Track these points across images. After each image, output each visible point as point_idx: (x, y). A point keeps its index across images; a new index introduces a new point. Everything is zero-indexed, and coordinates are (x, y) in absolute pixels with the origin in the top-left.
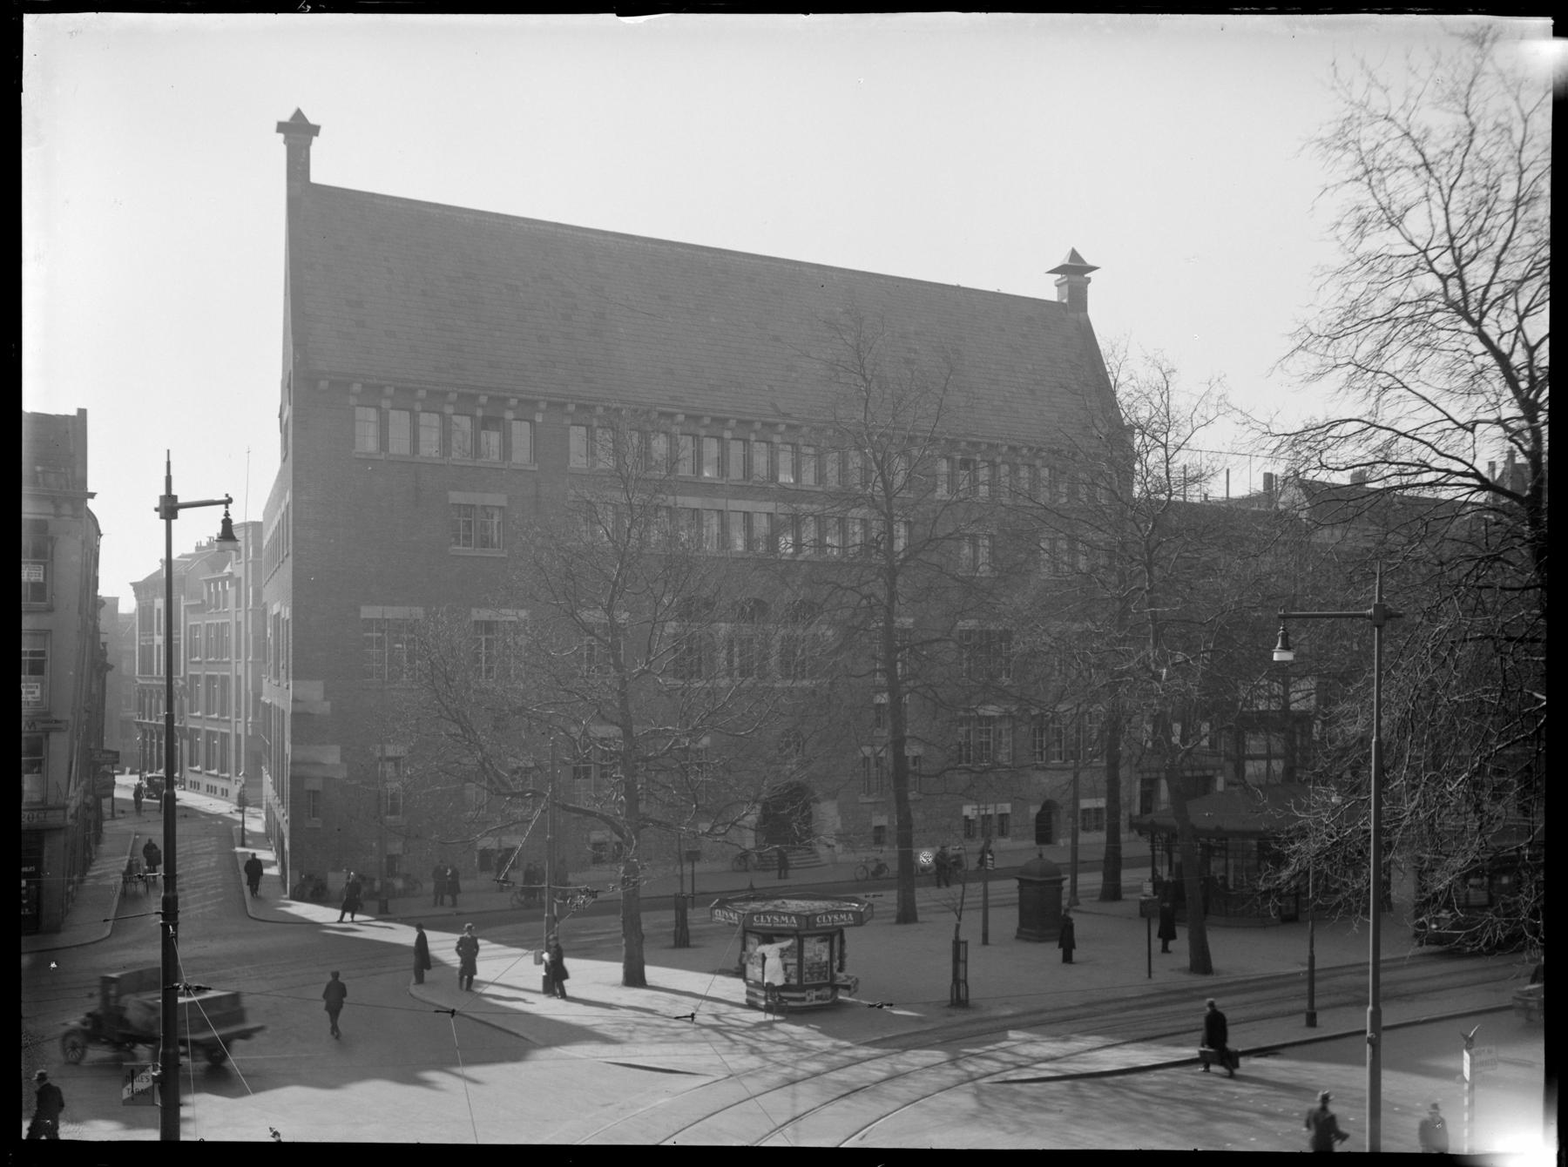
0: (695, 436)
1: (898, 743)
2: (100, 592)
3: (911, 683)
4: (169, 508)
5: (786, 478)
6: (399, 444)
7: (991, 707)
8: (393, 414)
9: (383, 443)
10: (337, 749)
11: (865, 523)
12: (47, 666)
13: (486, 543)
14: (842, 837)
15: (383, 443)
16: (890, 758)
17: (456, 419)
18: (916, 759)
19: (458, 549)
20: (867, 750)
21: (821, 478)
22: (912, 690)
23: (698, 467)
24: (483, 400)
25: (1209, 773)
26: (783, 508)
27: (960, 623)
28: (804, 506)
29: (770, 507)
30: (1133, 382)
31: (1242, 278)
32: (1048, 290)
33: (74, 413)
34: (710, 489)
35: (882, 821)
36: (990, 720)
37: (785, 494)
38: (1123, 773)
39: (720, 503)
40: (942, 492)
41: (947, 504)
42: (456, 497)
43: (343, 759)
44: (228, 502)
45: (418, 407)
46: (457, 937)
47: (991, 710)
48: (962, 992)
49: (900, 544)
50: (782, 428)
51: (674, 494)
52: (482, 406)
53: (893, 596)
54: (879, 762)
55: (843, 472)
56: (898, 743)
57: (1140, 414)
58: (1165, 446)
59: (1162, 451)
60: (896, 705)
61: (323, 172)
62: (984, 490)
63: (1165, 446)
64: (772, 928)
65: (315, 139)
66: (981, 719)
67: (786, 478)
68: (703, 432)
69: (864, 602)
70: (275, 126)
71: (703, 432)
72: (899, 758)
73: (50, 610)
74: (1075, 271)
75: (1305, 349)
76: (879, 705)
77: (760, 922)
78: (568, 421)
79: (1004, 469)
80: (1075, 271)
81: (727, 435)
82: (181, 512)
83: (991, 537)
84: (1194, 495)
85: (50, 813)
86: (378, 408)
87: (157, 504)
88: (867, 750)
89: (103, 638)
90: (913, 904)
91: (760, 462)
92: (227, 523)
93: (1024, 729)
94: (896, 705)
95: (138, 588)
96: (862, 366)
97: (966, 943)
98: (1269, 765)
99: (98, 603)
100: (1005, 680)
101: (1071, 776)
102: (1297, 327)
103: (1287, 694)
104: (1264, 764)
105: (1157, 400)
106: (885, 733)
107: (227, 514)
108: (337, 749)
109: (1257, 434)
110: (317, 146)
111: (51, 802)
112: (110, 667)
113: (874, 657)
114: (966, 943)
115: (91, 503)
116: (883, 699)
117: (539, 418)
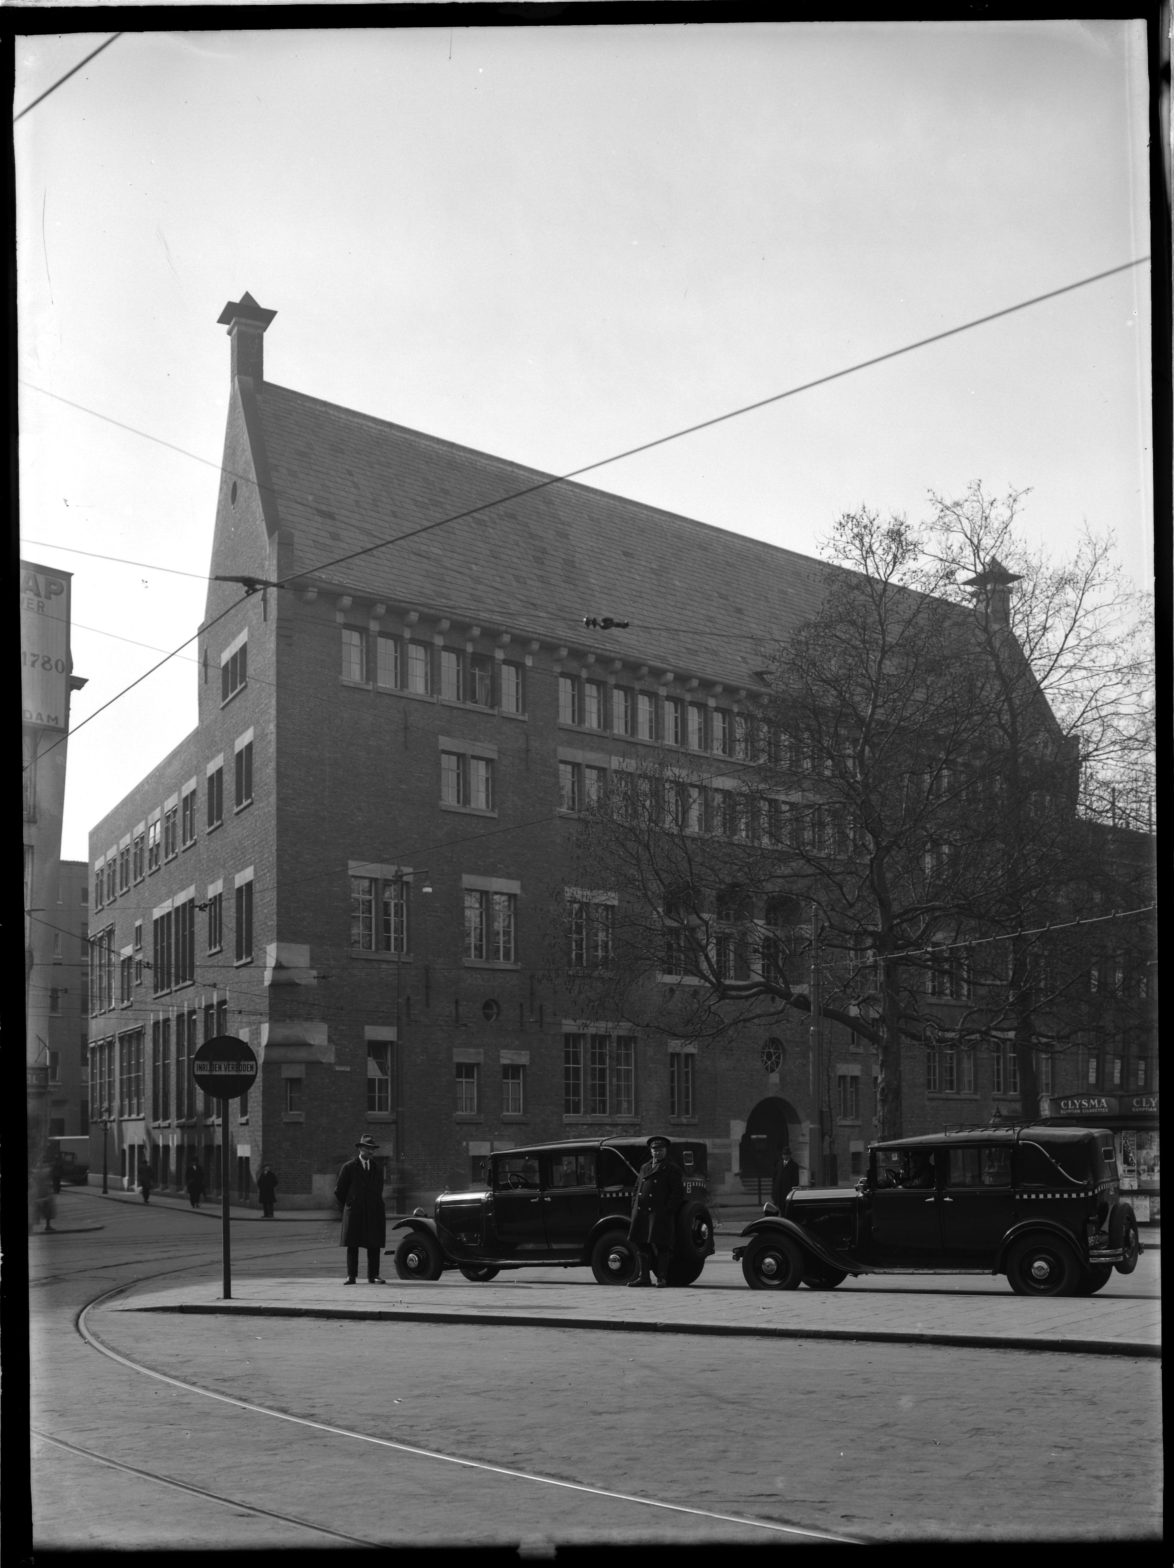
9: (370, 673)
34: (695, 761)
108: (324, 1027)
110: (271, 337)
117: (529, 662)
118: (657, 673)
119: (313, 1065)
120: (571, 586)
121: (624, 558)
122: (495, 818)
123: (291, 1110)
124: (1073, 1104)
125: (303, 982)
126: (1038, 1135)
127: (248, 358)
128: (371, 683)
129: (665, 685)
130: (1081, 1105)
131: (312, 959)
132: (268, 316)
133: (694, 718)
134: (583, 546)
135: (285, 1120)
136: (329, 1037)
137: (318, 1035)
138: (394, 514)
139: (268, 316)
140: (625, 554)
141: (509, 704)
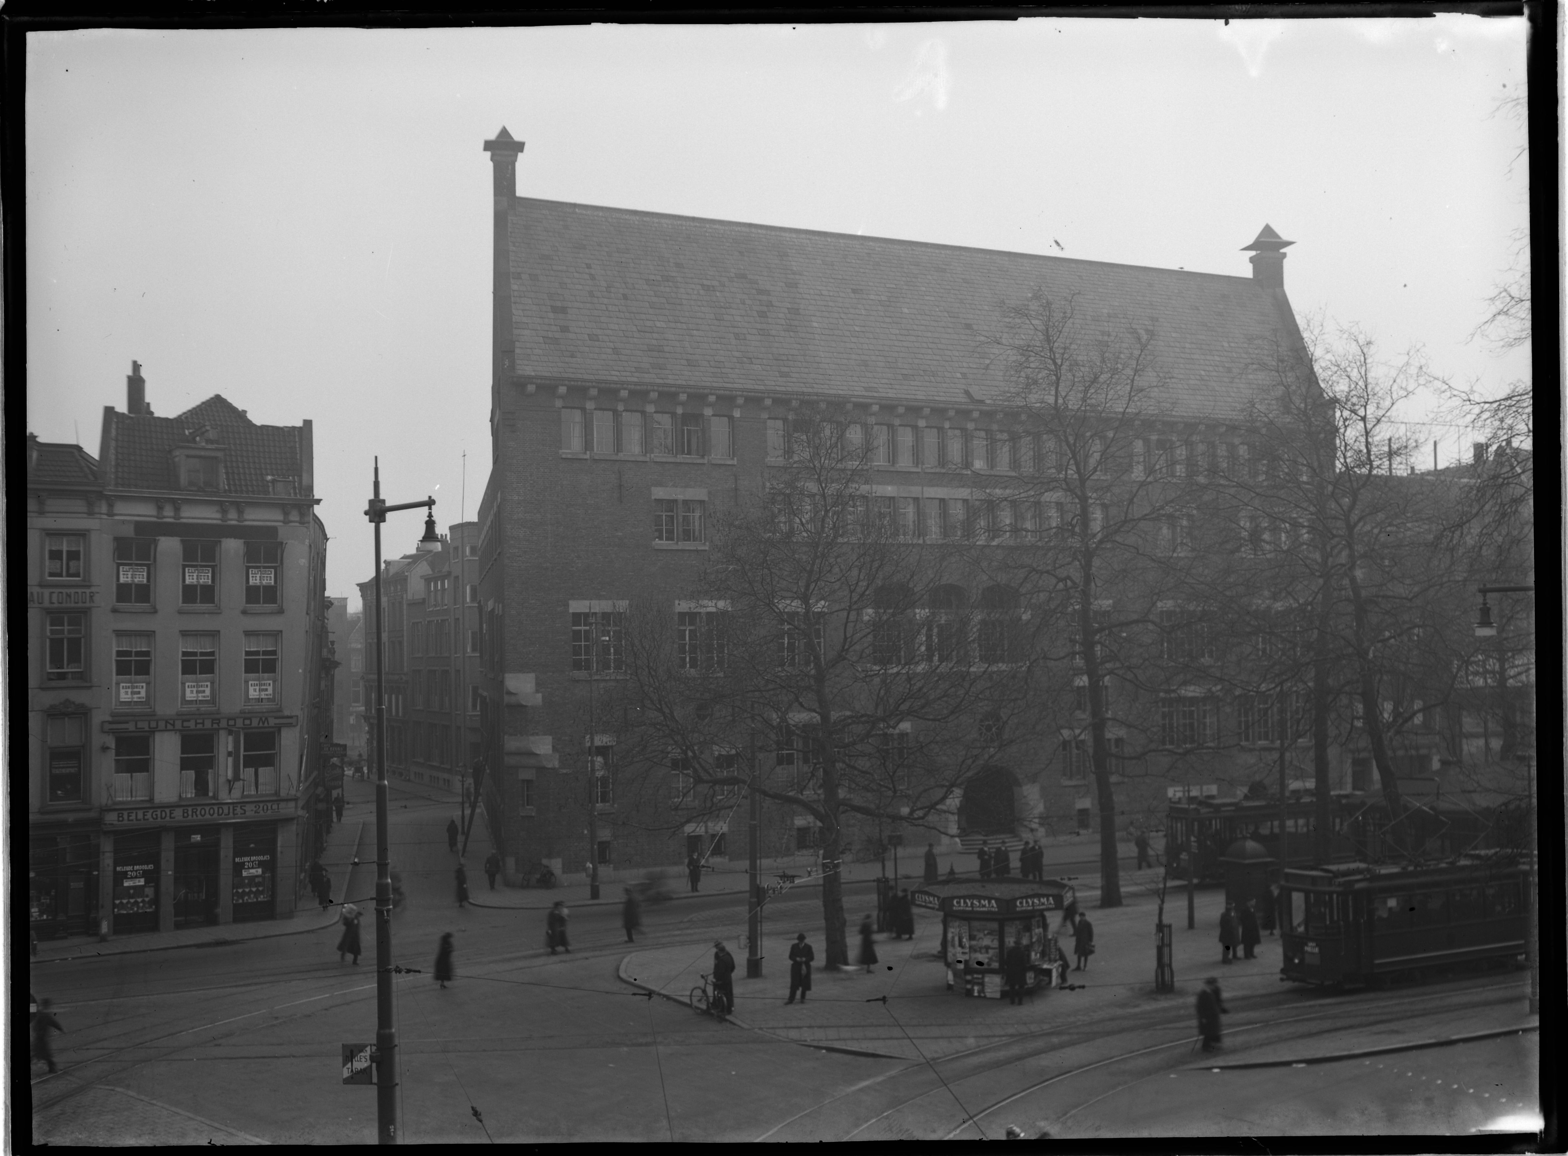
0: (890, 426)
1: (1098, 727)
2: (327, 594)
3: (1109, 665)
4: (377, 512)
5: (979, 464)
6: (602, 446)
7: (1192, 688)
8: (597, 414)
9: (588, 445)
10: (549, 739)
11: (1059, 505)
12: (278, 665)
13: (688, 535)
14: (1044, 820)
15: (588, 445)
16: (1090, 742)
17: (657, 417)
18: (1119, 741)
19: (663, 544)
20: (1066, 733)
21: (1015, 464)
22: (1111, 672)
23: (893, 458)
24: (683, 397)
25: (1423, 752)
26: (978, 494)
27: (1159, 604)
28: (998, 491)
29: (964, 493)
30: (1329, 356)
31: (1368, 228)
32: (1242, 267)
33: (300, 424)
34: (905, 477)
35: (1085, 803)
36: (1193, 701)
37: (979, 481)
38: (1332, 752)
39: (915, 491)
40: (1138, 473)
41: (1142, 484)
42: (659, 493)
43: (554, 748)
44: (430, 503)
45: (620, 407)
46: (1010, 876)
47: (1192, 691)
48: (1167, 977)
49: (1096, 525)
50: (976, 415)
51: (866, 482)
52: (682, 404)
53: (1088, 578)
54: (1080, 745)
55: (1039, 458)
56: (1098, 727)
57: (1337, 388)
58: (1364, 419)
59: (1361, 424)
60: (1095, 688)
61: (530, 183)
62: (1180, 470)
63: (1364, 419)
64: (972, 912)
65: (520, 155)
66: (1181, 700)
67: (979, 464)
68: (897, 422)
69: (1061, 585)
70: (482, 145)
71: (897, 422)
72: (1099, 739)
73: (281, 611)
74: (1269, 249)
75: (1506, 313)
76: (1079, 688)
77: (959, 906)
78: (765, 415)
79: (1201, 448)
80: (1269, 249)
81: (922, 423)
82: (389, 515)
83: (1190, 517)
84: (1401, 470)
85: (282, 805)
86: (583, 409)
87: (367, 507)
88: (1066, 733)
89: (331, 637)
90: (1117, 887)
91: (955, 449)
92: (430, 524)
93: (1228, 710)
94: (1095, 688)
95: (362, 587)
96: (1051, 350)
97: (1170, 926)
98: (1487, 743)
99: (326, 604)
100: (1206, 660)
101: (1276, 755)
102: (1497, 291)
103: (1503, 670)
104: (1481, 742)
105: (1355, 374)
106: (1084, 716)
107: (430, 515)
108: (549, 739)
109: (1456, 402)
110: (522, 163)
111: (283, 793)
112: (337, 664)
113: (1073, 641)
114: (1170, 926)
115: (317, 510)
116: (1083, 681)
117: (737, 414)
118: (864, 407)
119: (541, 770)
120: (792, 334)
121: (852, 295)
122: (705, 551)
124: (1027, 902)
125: (529, 704)
127: (504, 180)
128: (588, 452)
129: (874, 414)
130: (1033, 903)
131: (537, 684)
132: (520, 147)
134: (812, 292)
135: (522, 814)
136: (553, 747)
138: (625, 297)
139: (520, 147)
140: (854, 291)
141: (719, 454)
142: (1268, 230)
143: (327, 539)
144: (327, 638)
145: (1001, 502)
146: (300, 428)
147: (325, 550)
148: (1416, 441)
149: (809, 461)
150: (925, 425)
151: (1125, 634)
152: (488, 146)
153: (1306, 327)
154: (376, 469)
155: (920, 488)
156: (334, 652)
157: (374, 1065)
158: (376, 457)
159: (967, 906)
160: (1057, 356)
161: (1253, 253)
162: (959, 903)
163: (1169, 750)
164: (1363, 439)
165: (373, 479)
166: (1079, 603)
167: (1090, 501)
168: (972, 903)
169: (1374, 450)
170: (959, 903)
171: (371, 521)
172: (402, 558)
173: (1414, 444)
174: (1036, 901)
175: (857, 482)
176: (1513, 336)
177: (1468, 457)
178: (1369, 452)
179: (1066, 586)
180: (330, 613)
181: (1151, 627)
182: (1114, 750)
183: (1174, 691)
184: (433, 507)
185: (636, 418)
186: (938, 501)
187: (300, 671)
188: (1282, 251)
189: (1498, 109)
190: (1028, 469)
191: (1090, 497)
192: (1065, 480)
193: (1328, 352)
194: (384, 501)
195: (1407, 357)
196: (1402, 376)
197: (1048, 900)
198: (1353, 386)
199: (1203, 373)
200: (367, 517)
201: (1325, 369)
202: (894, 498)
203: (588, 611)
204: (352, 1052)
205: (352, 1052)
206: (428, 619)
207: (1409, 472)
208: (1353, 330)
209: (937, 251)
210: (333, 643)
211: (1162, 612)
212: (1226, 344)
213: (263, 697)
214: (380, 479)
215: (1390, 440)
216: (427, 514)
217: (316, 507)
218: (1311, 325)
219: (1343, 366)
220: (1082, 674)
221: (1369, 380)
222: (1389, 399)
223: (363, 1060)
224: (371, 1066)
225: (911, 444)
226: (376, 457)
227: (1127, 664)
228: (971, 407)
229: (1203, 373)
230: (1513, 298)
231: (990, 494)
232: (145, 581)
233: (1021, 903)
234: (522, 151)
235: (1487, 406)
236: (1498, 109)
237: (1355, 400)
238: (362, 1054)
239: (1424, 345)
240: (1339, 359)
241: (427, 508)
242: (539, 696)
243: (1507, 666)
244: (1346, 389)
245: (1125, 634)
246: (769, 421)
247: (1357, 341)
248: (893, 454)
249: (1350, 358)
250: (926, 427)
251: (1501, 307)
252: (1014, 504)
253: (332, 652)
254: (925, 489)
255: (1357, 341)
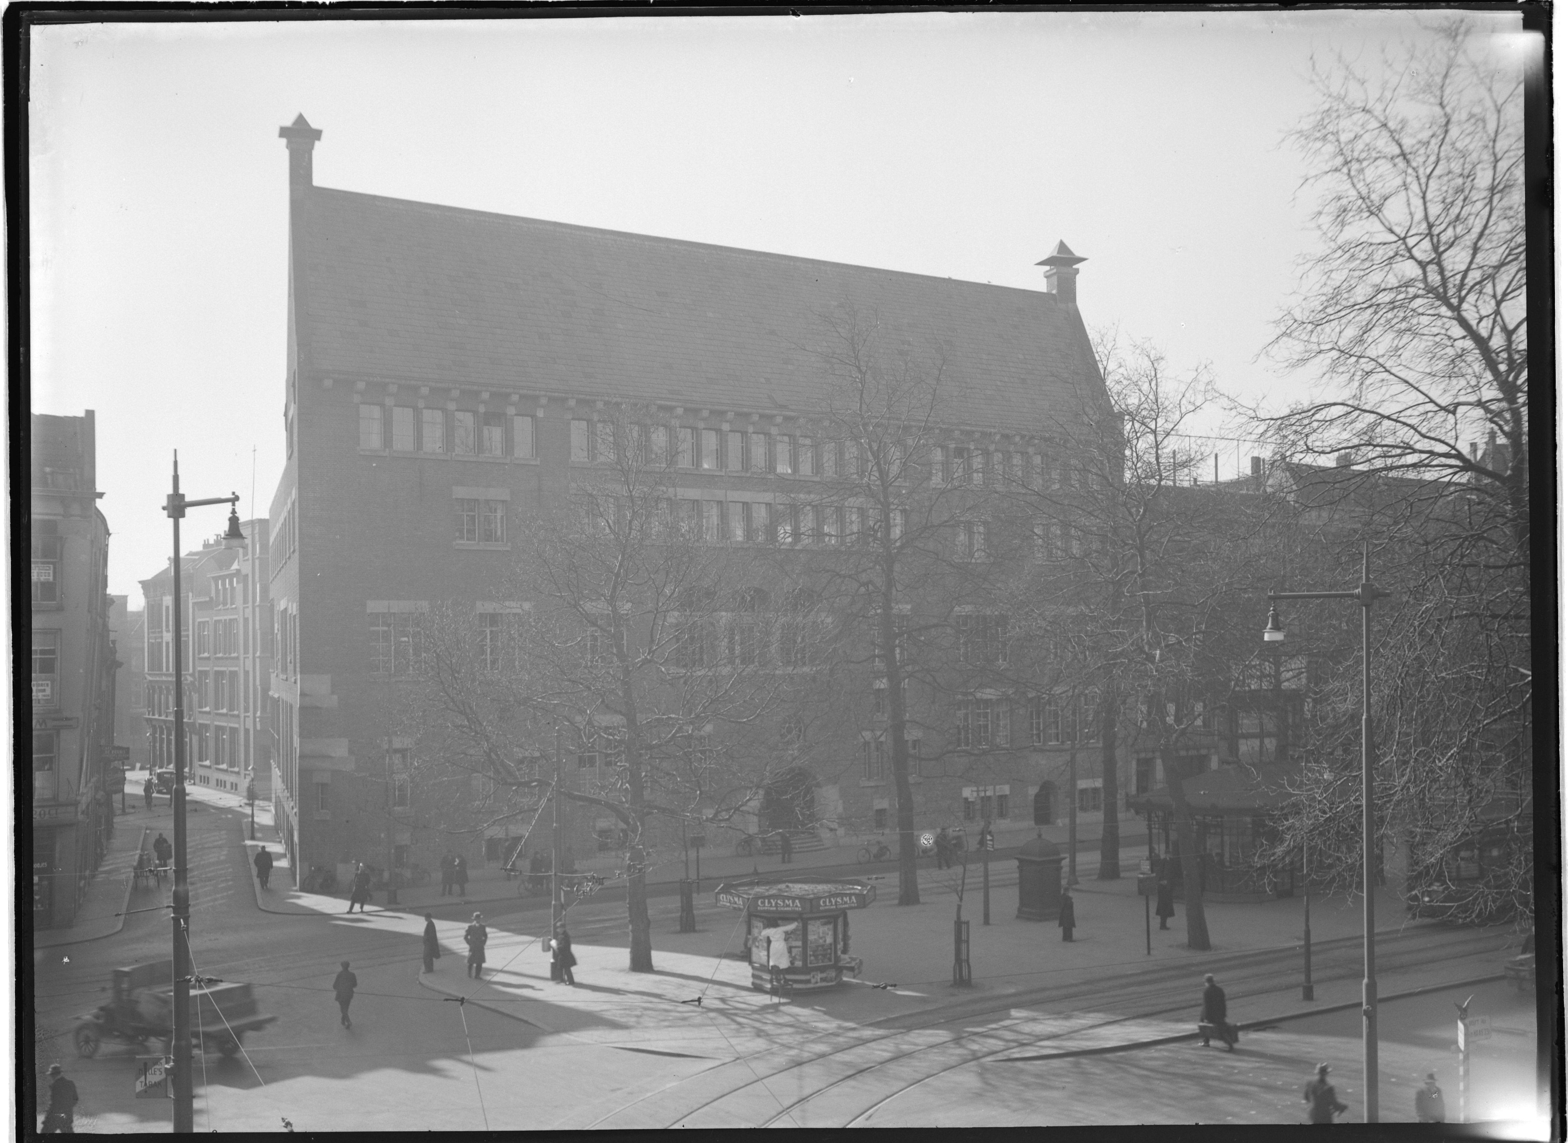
1: (898, 728)
3: (909, 668)
4: (177, 507)
5: (784, 468)
7: (988, 690)
8: (397, 411)
9: (387, 440)
11: (862, 512)
13: (489, 536)
15: (387, 440)
17: (460, 415)
18: (915, 743)
20: (867, 735)
21: (818, 467)
25: (1204, 752)
29: (768, 497)
30: (1122, 370)
32: (1037, 281)
33: (81, 414)
34: (710, 480)
36: (987, 703)
37: (784, 485)
38: (1119, 753)
39: (719, 494)
42: (460, 492)
44: (235, 499)
47: (989, 694)
48: (965, 972)
56: (898, 728)
58: (1154, 432)
62: (978, 478)
63: (1154, 432)
65: (317, 143)
67: (784, 468)
68: (701, 425)
69: (863, 589)
70: (277, 131)
71: (701, 425)
73: (60, 609)
75: (1289, 335)
76: (879, 690)
77: (764, 906)
81: (726, 427)
82: (189, 511)
83: (985, 523)
86: (382, 405)
87: (165, 503)
88: (867, 735)
89: (112, 636)
91: (758, 453)
96: (856, 358)
97: (967, 923)
99: (108, 602)
102: (1281, 314)
103: (1278, 673)
104: (1256, 743)
105: (1145, 387)
107: (234, 512)
110: (319, 151)
112: (120, 665)
114: (967, 923)
115: (99, 503)
116: (882, 684)
117: (540, 414)
123: (322, 808)
124: (830, 901)
126: (789, 924)
130: (836, 902)
133: (734, 442)
137: (339, 749)
142: (301, 120)
143: (109, 535)
144: (108, 636)
145: (805, 506)
146: (81, 418)
147: (107, 545)
148: (1202, 454)
149: (617, 463)
150: (729, 429)
151: (923, 638)
152: (284, 132)
153: (1100, 341)
154: (176, 463)
155: (724, 491)
156: (116, 652)
157: (169, 1078)
158: (175, 450)
159: (771, 906)
160: (862, 363)
161: (1047, 268)
162: (763, 903)
163: (964, 751)
164: (1153, 451)
165: (172, 473)
166: (880, 607)
167: (892, 507)
168: (776, 903)
169: (1162, 460)
170: (763, 903)
171: (169, 516)
172: (187, 555)
173: (1200, 457)
174: (839, 900)
175: (664, 485)
176: (1296, 357)
177: (1247, 470)
178: (1158, 463)
179: (868, 590)
180: (112, 612)
181: (949, 630)
182: (912, 752)
183: (971, 693)
184: (237, 503)
185: (438, 415)
186: (741, 505)
187: (81, 671)
188: (1075, 266)
189: (1283, 140)
190: (829, 472)
191: (893, 503)
192: (868, 485)
193: (1120, 366)
194: (183, 496)
195: (1195, 374)
196: (1190, 391)
197: (850, 899)
198: (1143, 399)
199: (999, 383)
200: (166, 512)
201: (1118, 382)
202: (697, 501)
203: (386, 611)
204: (145, 1064)
205: (145, 1064)
206: (215, 618)
207: (1192, 483)
208: (1146, 346)
209: (742, 256)
210: (114, 642)
211: (959, 617)
212: (1021, 356)
213: (40, 697)
214: (180, 472)
215: (1174, 452)
216: (230, 510)
217: (98, 501)
218: (1105, 340)
219: (1134, 379)
220: (883, 677)
221: (1160, 395)
222: (1178, 413)
223: (158, 1073)
224: (166, 1079)
225: (715, 448)
226: (175, 450)
227: (926, 667)
228: (775, 412)
229: (999, 383)
230: (1296, 321)
231: (794, 499)
232: (51, 578)
233: (824, 902)
234: (319, 139)
235: (1272, 422)
236: (1283, 140)
237: (1144, 413)
238: (157, 1067)
239: (1212, 363)
240: (1131, 373)
241: (230, 504)
242: (335, 697)
243: (1282, 669)
244: (1136, 402)
245: (923, 638)
246: (456, 413)
247: (1149, 356)
248: (697, 457)
249: (1142, 373)
250: (731, 431)
251: (1284, 329)
252: (817, 509)
253: (114, 651)
254: (728, 492)
255: (1149, 356)
